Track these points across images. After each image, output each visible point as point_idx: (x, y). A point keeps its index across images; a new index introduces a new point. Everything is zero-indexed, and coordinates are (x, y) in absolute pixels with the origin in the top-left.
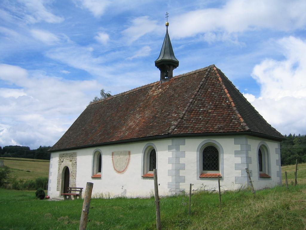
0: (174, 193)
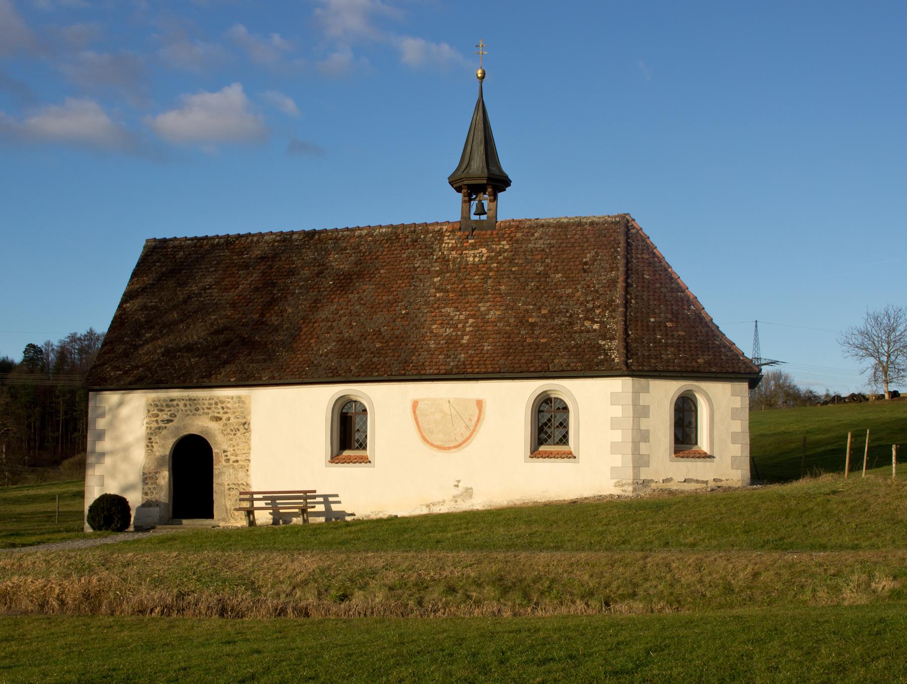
0: (629, 491)
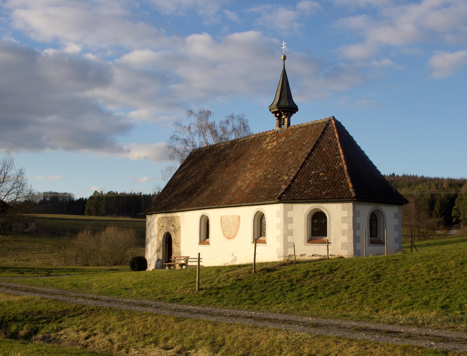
0: (282, 259)
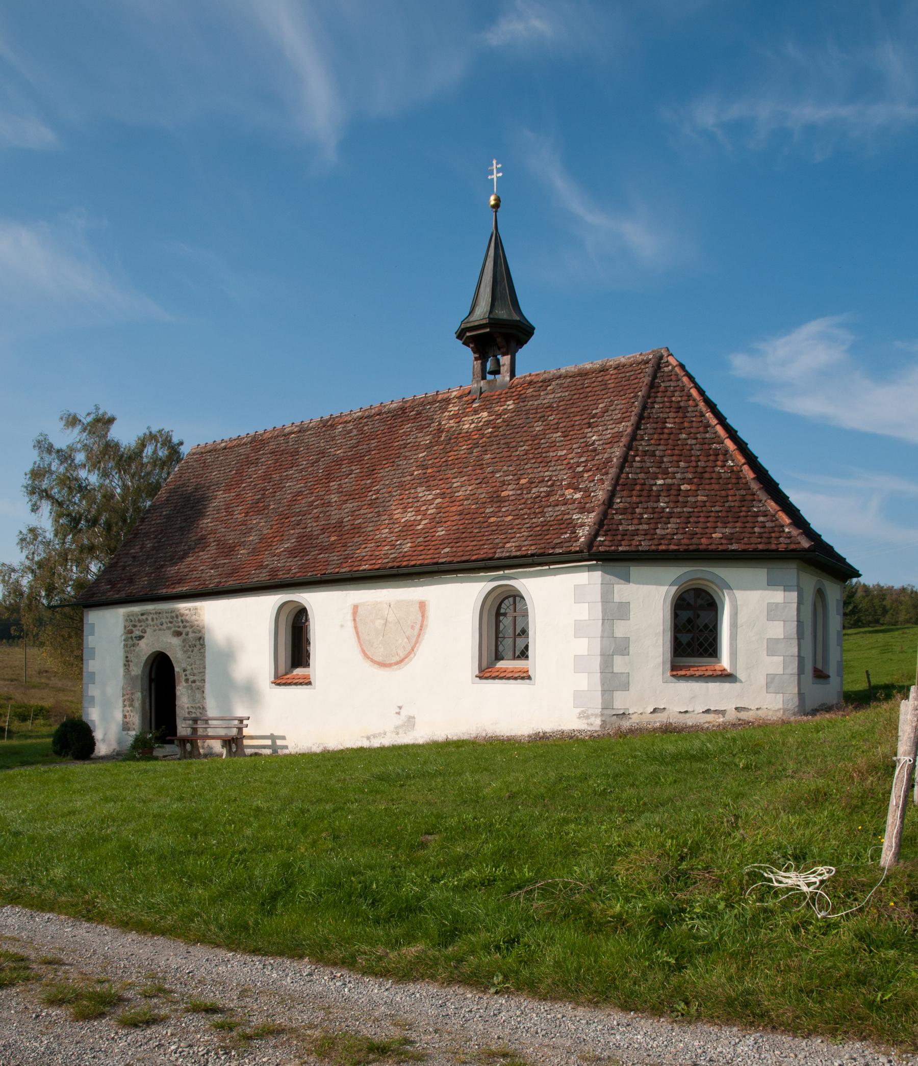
0: (595, 724)
